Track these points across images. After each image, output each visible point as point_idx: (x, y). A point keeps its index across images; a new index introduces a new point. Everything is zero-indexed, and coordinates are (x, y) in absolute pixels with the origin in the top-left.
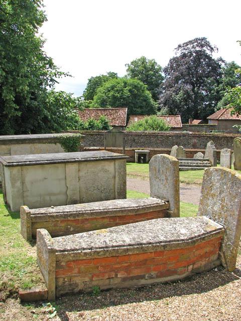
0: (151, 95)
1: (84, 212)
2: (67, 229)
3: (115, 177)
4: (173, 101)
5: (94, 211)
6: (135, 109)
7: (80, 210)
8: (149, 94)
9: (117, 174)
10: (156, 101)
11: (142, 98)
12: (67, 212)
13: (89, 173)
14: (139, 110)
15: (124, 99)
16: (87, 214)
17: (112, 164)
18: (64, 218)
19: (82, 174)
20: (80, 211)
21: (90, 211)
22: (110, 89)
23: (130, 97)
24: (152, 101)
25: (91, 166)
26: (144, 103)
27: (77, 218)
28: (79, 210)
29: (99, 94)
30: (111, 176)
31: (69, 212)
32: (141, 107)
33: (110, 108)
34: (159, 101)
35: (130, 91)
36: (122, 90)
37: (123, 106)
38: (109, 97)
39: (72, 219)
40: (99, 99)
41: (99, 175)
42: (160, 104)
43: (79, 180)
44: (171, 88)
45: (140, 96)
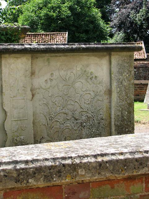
0: (100, 14)
1: (78, 161)
2: (113, 195)
3: (109, 92)
4: (132, 23)
5: (106, 159)
6: (77, 35)
7: (63, 155)
8: (96, 12)
9: (115, 84)
10: (107, 24)
11: (87, 19)
12: (27, 162)
13: (54, 83)
14: (83, 35)
15: (62, 19)
16: (87, 167)
17: (104, 62)
18: (17, 181)
19: (40, 81)
20: (64, 158)
21: (95, 156)
22: (41, 6)
23: (70, 17)
24: (102, 23)
25: (59, 64)
26: (91, 26)
27: (56, 181)
28: (59, 155)
29: (26, 13)
30: (102, 88)
31: (33, 161)
32: (87, 32)
33: (43, 32)
34: (112, 24)
35: (70, 8)
36: (59, 7)
37: (61, 29)
38: (40, 18)
39: (41, 184)
40: (27, 20)
41: (78, 85)
42: (112, 27)
43: (33, 95)
44: (127, 4)
45: (85, 15)
